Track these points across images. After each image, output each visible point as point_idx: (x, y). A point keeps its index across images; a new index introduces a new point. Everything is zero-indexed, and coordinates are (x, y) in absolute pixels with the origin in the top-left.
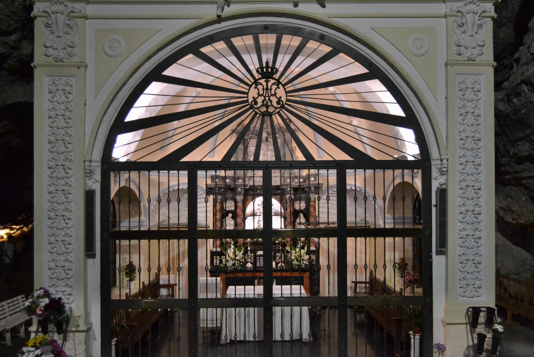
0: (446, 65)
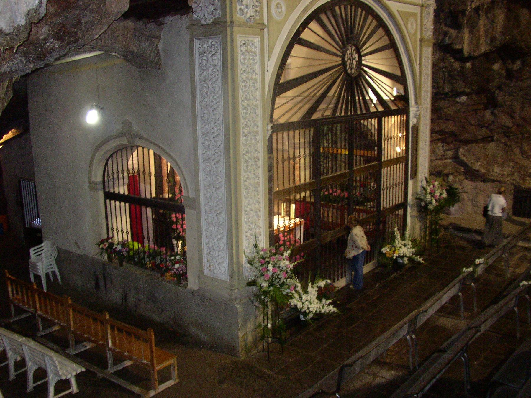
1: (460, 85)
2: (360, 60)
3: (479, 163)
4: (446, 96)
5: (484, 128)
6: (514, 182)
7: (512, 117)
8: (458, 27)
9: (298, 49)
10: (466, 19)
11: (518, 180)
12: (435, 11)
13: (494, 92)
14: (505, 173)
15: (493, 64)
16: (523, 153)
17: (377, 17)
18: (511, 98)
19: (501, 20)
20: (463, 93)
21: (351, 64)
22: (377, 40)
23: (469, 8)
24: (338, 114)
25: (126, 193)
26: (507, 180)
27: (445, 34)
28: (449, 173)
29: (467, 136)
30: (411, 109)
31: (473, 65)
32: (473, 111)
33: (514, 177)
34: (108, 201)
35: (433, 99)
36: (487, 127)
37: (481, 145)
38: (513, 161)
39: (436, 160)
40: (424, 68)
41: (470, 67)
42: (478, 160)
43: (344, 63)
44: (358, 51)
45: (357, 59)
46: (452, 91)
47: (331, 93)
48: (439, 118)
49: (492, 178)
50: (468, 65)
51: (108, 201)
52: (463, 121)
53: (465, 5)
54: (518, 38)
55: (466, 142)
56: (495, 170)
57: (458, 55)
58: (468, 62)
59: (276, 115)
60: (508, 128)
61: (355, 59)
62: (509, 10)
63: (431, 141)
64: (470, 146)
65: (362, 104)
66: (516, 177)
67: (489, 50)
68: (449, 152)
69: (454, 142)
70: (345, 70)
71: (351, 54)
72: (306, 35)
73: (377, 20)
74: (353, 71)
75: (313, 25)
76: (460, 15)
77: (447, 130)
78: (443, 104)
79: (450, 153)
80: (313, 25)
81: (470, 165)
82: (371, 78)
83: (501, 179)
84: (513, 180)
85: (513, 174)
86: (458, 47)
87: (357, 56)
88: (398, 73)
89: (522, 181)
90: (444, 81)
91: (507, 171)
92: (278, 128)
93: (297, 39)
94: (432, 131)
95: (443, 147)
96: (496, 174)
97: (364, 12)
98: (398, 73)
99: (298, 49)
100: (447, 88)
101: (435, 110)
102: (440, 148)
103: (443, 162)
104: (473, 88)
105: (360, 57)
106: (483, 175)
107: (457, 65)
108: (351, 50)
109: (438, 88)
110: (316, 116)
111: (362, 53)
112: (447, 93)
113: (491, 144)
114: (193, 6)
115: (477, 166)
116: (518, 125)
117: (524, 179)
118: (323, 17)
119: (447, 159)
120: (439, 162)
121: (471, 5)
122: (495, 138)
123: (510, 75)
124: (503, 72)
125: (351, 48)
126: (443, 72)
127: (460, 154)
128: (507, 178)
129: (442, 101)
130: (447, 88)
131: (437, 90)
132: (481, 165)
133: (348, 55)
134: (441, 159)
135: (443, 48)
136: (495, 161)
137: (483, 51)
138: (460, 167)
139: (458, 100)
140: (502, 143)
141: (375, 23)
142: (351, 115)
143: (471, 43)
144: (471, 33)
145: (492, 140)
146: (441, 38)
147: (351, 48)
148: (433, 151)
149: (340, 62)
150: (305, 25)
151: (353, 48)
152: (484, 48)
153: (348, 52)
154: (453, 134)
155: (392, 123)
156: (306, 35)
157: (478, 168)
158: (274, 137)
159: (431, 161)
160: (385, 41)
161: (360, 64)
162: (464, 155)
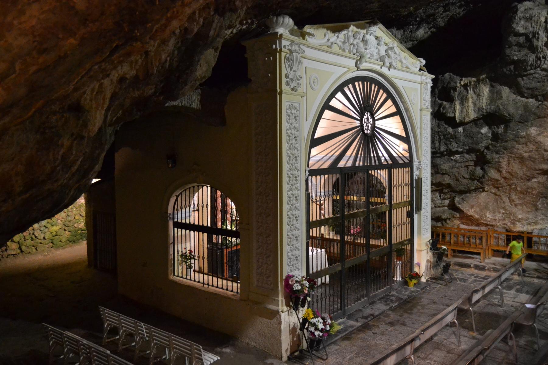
0: (421, 110)
1: (454, 146)
2: (374, 123)
3: (473, 210)
4: (442, 154)
5: (476, 181)
6: (505, 226)
7: (500, 172)
8: (451, 100)
9: (327, 114)
10: (457, 93)
11: (509, 224)
12: (432, 87)
13: (484, 151)
14: (497, 218)
15: (481, 128)
16: (512, 201)
17: (386, 91)
18: (498, 156)
19: (486, 94)
20: (457, 152)
21: (367, 126)
22: (389, 108)
23: (459, 85)
24: (357, 164)
25: (505, 70)
26: (498, 224)
27: (440, 105)
28: (447, 218)
29: (462, 188)
30: (415, 163)
31: (464, 130)
32: (465, 167)
33: (505, 222)
34: (176, 229)
35: (432, 157)
36: (478, 180)
37: (474, 195)
38: (504, 208)
39: (435, 207)
40: (423, 131)
41: (462, 131)
42: (472, 207)
43: (362, 125)
44: (373, 117)
45: (371, 123)
46: (447, 151)
47: (349, 153)
48: (437, 173)
49: (485, 222)
50: (460, 129)
51: (176, 229)
52: (457, 175)
53: (456, 83)
54: (501, 107)
55: (461, 192)
56: (488, 216)
57: (452, 122)
58: (459, 126)
59: (312, 161)
60: (498, 180)
61: (370, 123)
62: (492, 86)
63: (432, 191)
64: (463, 196)
65: (376, 158)
66: (506, 221)
67: (477, 117)
68: (446, 201)
69: (450, 193)
70: (363, 131)
71: (367, 119)
72: (334, 103)
73: (386, 93)
74: (369, 132)
75: (339, 95)
76: (452, 91)
77: (444, 183)
78: (438, 161)
79: (447, 202)
80: (339, 95)
81: (465, 211)
82: (383, 138)
83: (494, 223)
84: (504, 224)
85: (504, 220)
86: (451, 115)
87: (371, 120)
88: (404, 135)
89: (512, 225)
90: (440, 142)
91: (498, 216)
92: (314, 173)
93: (327, 106)
94: (432, 184)
95: (440, 196)
96: (489, 219)
97: (377, 87)
98: (404, 135)
99: (327, 114)
100: (443, 148)
101: (434, 166)
102: (439, 197)
103: (441, 209)
104: (465, 148)
105: (374, 121)
106: (477, 219)
107: (450, 130)
108: (367, 115)
109: (435, 148)
110: (341, 164)
111: (376, 118)
112: (443, 152)
113: (482, 194)
114: (252, 79)
115: (471, 212)
116: (505, 178)
117: (514, 224)
118: (346, 90)
119: (444, 206)
120: (438, 209)
121: (460, 83)
122: (485, 189)
123: (496, 137)
124: (490, 135)
125: (367, 114)
126: (439, 136)
127: (456, 202)
128: (499, 222)
129: (439, 159)
130: (443, 148)
131: (434, 150)
132: (475, 211)
133: (364, 119)
134: (439, 207)
135: (438, 115)
136: (486, 208)
137: (472, 118)
138: (456, 213)
139: (452, 158)
140: (492, 193)
141: (385, 95)
142: (367, 166)
143: (462, 112)
144: (462, 104)
145: (484, 191)
146: (436, 109)
147: (367, 114)
148: (433, 200)
149: (359, 125)
150: (332, 95)
151: (369, 114)
152: (473, 115)
153: (365, 117)
154: (449, 186)
155: (400, 176)
156: (334, 103)
157: (472, 214)
158: (310, 177)
159: (432, 208)
160: (393, 109)
161: (374, 127)
162: (459, 204)
